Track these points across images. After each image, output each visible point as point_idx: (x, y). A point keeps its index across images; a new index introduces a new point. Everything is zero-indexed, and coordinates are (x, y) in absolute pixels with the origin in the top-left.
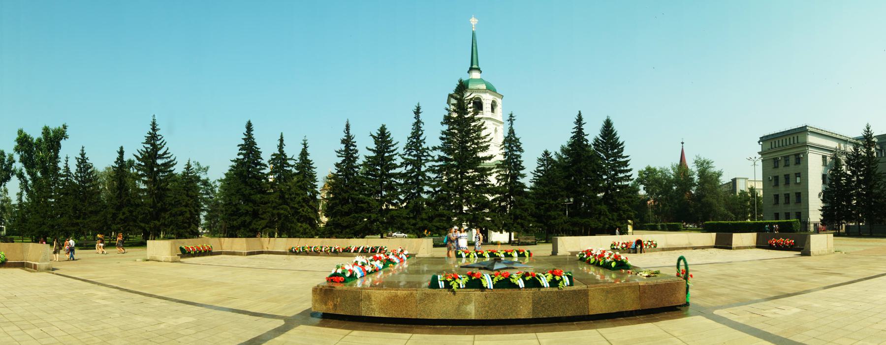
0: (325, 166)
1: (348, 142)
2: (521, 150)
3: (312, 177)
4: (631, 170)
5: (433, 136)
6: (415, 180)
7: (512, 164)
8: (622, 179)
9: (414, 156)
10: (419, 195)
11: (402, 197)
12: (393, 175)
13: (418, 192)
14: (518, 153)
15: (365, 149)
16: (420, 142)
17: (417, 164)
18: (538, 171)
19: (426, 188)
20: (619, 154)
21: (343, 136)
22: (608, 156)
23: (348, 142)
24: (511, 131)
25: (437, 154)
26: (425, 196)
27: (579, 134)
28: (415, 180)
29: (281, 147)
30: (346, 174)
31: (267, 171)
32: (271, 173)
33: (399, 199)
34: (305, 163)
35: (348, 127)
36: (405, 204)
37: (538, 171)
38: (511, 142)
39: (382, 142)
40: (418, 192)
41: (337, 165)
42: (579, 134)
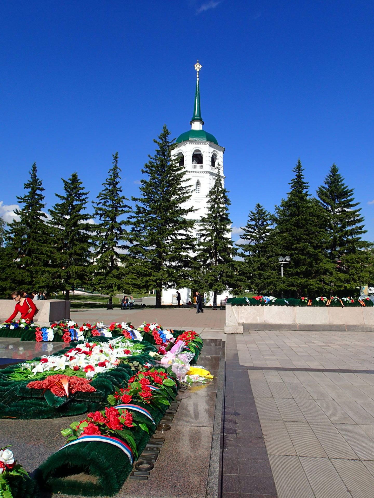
1: (34, 185)
8: (352, 233)
18: (249, 226)
21: (28, 179)
35: (34, 169)
37: (249, 226)
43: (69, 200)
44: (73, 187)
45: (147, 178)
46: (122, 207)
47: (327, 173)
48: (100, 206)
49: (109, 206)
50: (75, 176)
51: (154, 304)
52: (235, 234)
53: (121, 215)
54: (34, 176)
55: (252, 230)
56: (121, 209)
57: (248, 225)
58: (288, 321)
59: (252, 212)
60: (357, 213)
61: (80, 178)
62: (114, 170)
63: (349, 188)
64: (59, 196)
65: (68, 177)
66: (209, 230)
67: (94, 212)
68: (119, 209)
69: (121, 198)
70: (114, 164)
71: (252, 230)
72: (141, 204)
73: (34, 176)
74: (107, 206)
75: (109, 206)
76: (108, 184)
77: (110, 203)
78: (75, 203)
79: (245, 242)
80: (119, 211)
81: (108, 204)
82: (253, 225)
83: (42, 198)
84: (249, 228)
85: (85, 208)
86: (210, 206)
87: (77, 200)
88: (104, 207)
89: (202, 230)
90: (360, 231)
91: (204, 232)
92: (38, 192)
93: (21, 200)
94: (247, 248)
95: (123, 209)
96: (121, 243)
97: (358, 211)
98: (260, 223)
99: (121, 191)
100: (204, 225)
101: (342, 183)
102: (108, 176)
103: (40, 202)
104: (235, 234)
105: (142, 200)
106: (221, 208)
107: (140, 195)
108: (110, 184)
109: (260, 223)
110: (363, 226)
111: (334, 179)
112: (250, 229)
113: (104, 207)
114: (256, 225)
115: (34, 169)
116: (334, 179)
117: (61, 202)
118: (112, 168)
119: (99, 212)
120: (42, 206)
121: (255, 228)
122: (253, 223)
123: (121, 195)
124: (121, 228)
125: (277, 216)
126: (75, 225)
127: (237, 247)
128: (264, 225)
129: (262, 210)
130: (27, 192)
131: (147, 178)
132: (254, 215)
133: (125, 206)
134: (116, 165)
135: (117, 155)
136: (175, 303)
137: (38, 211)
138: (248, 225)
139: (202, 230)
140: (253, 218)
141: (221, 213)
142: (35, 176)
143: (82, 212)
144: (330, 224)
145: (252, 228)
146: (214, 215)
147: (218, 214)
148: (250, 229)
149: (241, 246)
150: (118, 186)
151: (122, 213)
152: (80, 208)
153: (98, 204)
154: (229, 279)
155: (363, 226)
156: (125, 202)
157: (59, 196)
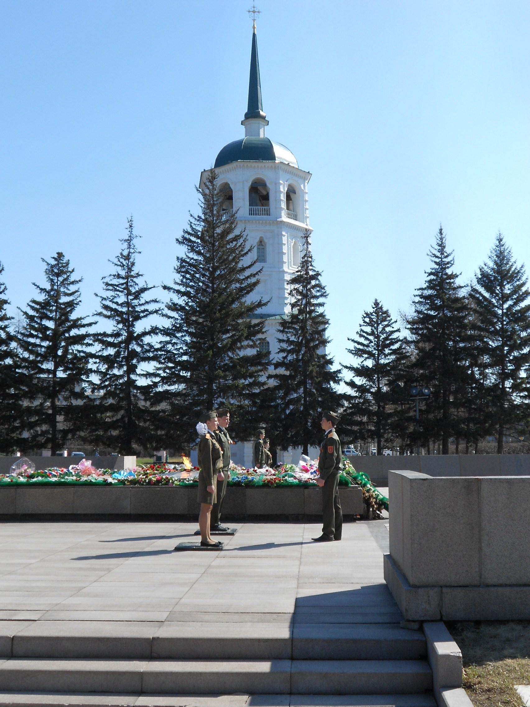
6: (127, 349)
12: (79, 340)
14: (321, 300)
17: (128, 317)
25: (167, 297)
28: (127, 349)
36: (102, 392)
43: (54, 294)
44: (59, 269)
46: (143, 304)
49: (121, 305)
52: (341, 349)
55: (366, 342)
56: (143, 308)
62: (129, 241)
63: (518, 266)
66: (292, 343)
71: (366, 342)
74: (117, 303)
75: (121, 305)
77: (122, 299)
78: (64, 299)
79: (356, 362)
94: (361, 372)
100: (287, 333)
107: (173, 278)
109: (380, 329)
113: (114, 306)
114: (372, 334)
117: (41, 298)
123: (141, 283)
126: (131, 338)
129: (381, 308)
131: (183, 251)
132: (368, 315)
136: (444, 590)
145: (367, 339)
146: (300, 317)
147: (308, 316)
152: (71, 305)
154: (262, 388)
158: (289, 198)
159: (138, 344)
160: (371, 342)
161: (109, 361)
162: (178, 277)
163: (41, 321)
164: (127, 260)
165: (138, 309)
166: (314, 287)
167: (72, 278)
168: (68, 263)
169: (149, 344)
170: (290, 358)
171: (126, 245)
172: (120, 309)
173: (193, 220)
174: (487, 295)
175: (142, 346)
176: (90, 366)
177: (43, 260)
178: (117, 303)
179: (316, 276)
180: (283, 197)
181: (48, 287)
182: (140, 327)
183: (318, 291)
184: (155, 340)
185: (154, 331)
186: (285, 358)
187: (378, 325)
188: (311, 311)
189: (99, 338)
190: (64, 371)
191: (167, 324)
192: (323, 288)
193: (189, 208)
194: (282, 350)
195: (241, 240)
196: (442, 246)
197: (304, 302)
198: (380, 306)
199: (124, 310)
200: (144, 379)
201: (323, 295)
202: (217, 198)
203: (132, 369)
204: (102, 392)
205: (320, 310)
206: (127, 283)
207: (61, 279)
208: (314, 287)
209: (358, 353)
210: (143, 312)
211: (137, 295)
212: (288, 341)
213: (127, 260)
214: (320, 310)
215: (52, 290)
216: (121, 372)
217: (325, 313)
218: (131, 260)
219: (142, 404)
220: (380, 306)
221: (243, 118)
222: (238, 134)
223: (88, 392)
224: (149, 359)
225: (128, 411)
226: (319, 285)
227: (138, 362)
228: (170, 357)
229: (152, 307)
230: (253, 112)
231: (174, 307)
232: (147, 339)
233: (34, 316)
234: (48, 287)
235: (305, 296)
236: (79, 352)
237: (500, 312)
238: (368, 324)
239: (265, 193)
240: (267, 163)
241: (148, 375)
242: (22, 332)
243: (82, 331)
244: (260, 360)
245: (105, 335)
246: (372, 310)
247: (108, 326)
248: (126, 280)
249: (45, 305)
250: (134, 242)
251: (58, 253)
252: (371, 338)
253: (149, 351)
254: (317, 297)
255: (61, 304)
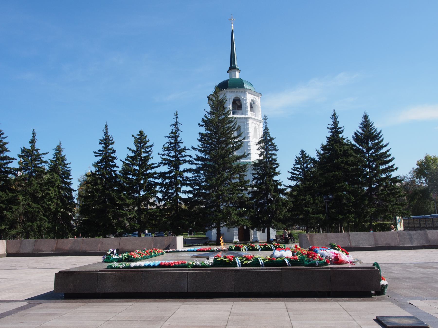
0: (81, 167)
1: (107, 141)
2: (276, 150)
3: (67, 174)
4: (393, 159)
5: (191, 139)
6: (174, 181)
7: (267, 167)
8: (384, 171)
9: (173, 157)
10: (177, 195)
11: (160, 195)
12: (151, 175)
13: (176, 191)
14: (274, 152)
15: (123, 152)
16: (177, 142)
17: (175, 164)
18: (296, 169)
19: (186, 166)
20: (378, 147)
21: (102, 136)
22: (369, 149)
23: (107, 141)
24: (266, 132)
25: (194, 154)
26: (184, 196)
27: (335, 131)
28: (174, 181)
29: (33, 142)
30: (103, 179)
31: (14, 165)
32: (20, 169)
33: (157, 198)
34: (59, 158)
35: (106, 127)
36: (163, 202)
37: (296, 169)
38: (267, 142)
39: (140, 143)
40: (176, 191)
41: (96, 165)
42: (335, 131)
43: (138, 153)
44: (141, 140)
45: (203, 130)
46: (183, 157)
47: (361, 119)
48: (165, 157)
50: (141, 132)
51: (266, 241)
52: (285, 178)
53: (184, 164)
54: (106, 133)
55: (298, 173)
57: (295, 167)
58: (208, 249)
59: (297, 157)
60: (388, 153)
61: (146, 133)
62: (175, 125)
64: (130, 149)
65: (136, 133)
67: (160, 161)
68: (181, 159)
69: (184, 149)
70: (175, 120)
71: (298, 173)
72: (199, 154)
73: (106, 133)
74: (170, 156)
76: (171, 137)
77: (173, 154)
78: (144, 155)
79: (293, 183)
80: (181, 160)
81: (171, 155)
82: (298, 168)
83: (114, 152)
84: (294, 170)
85: (152, 158)
86: (260, 153)
87: (144, 153)
88: (169, 158)
89: (255, 174)
90: (391, 169)
91: (256, 176)
92: (111, 146)
93: (97, 154)
95: (185, 158)
96: (184, 188)
97: (388, 151)
98: (305, 166)
99: (182, 143)
101: (373, 126)
102: (169, 130)
103: (113, 155)
104: (285, 178)
105: (200, 151)
106: (270, 154)
107: (197, 144)
108: (172, 137)
110: (394, 165)
111: (366, 124)
112: (296, 172)
113: (169, 158)
115: (106, 127)
116: (366, 124)
117: (133, 154)
118: (174, 123)
119: (164, 162)
120: (115, 158)
121: (301, 171)
122: (299, 166)
123: (182, 146)
124: (183, 175)
125: (317, 159)
127: (286, 188)
128: (308, 168)
130: (101, 147)
131: (203, 130)
132: (299, 159)
133: (185, 156)
134: (177, 120)
135: (177, 112)
137: (111, 163)
138: (295, 167)
139: (255, 174)
140: (298, 161)
141: (270, 159)
142: (107, 132)
143: (150, 162)
144: (377, 204)
145: (299, 171)
148: (296, 172)
149: (290, 187)
150: (179, 139)
151: (183, 163)
152: (147, 158)
153: (163, 155)
155: (394, 165)
156: (188, 153)
157: (130, 149)
158: (251, 107)
159: (181, 177)
160: (300, 173)
161: (166, 186)
162: (200, 143)
163: (132, 166)
164: (175, 136)
165: (181, 159)
166: (270, 145)
167: (148, 144)
168: (146, 137)
169: (186, 177)
170: (259, 182)
171: (173, 127)
172: (171, 159)
173: (207, 114)
174: (361, 147)
175: (183, 178)
176: (157, 189)
177: (133, 136)
178: (170, 156)
179: (271, 139)
180: (248, 106)
181: (135, 149)
182: (182, 168)
183: (272, 147)
184: (189, 175)
185: (190, 170)
186: (256, 182)
187: (304, 164)
188: (269, 158)
189: (162, 175)
190: (144, 191)
191: (194, 167)
192: (275, 146)
193: (204, 109)
194: (255, 178)
195: (233, 124)
196: (336, 123)
197: (265, 153)
198: (305, 153)
199: (174, 159)
200: (184, 194)
201: (276, 150)
202: (217, 105)
203: (178, 190)
204: (163, 202)
205: (274, 157)
206: (175, 146)
207: (142, 145)
208: (270, 145)
209: (292, 179)
210: (183, 160)
211: (180, 152)
212: (258, 173)
213: (175, 136)
214: (274, 157)
215: (137, 150)
216: (173, 191)
217: (277, 159)
218: (177, 135)
219: (183, 207)
220: (305, 153)
221: (228, 69)
222: (226, 77)
223: (157, 203)
224: (187, 185)
225: (176, 211)
226: (272, 144)
227: (181, 186)
228: (198, 184)
229: (187, 159)
230: (233, 67)
231: (199, 158)
232: (185, 174)
233: (129, 164)
234: (135, 149)
235: (266, 150)
236: (151, 181)
237: (367, 155)
238: (299, 164)
239: (239, 105)
240: (242, 90)
241: (186, 192)
242: (43, 164)
243: (153, 171)
244: (243, 183)
245: (165, 173)
246: (300, 156)
247: (165, 169)
248: (174, 144)
249: (134, 158)
250: (179, 125)
251: (140, 132)
252: (301, 171)
253: (187, 181)
254: (272, 151)
255: (142, 157)
